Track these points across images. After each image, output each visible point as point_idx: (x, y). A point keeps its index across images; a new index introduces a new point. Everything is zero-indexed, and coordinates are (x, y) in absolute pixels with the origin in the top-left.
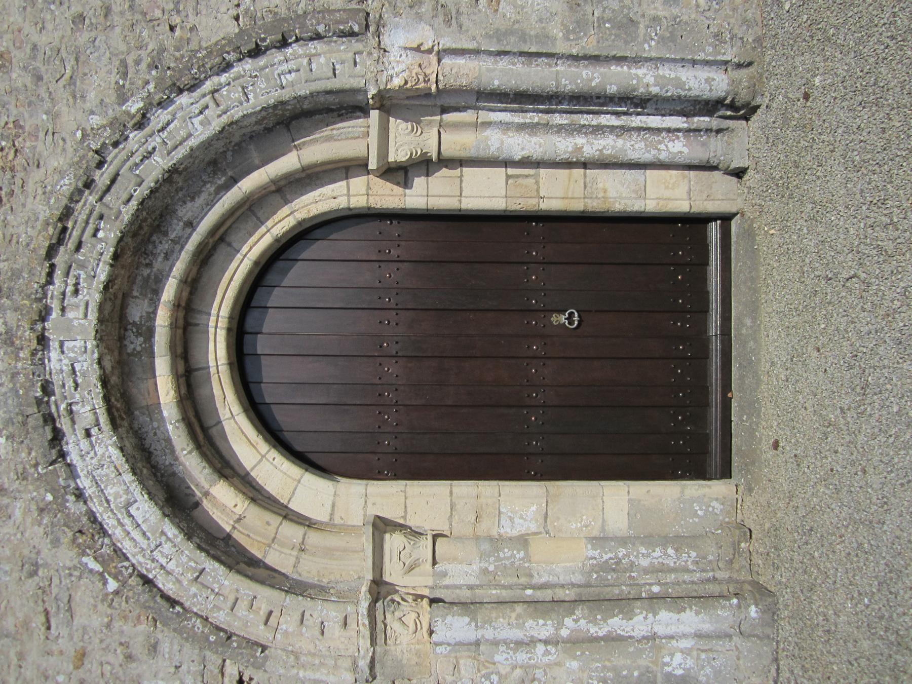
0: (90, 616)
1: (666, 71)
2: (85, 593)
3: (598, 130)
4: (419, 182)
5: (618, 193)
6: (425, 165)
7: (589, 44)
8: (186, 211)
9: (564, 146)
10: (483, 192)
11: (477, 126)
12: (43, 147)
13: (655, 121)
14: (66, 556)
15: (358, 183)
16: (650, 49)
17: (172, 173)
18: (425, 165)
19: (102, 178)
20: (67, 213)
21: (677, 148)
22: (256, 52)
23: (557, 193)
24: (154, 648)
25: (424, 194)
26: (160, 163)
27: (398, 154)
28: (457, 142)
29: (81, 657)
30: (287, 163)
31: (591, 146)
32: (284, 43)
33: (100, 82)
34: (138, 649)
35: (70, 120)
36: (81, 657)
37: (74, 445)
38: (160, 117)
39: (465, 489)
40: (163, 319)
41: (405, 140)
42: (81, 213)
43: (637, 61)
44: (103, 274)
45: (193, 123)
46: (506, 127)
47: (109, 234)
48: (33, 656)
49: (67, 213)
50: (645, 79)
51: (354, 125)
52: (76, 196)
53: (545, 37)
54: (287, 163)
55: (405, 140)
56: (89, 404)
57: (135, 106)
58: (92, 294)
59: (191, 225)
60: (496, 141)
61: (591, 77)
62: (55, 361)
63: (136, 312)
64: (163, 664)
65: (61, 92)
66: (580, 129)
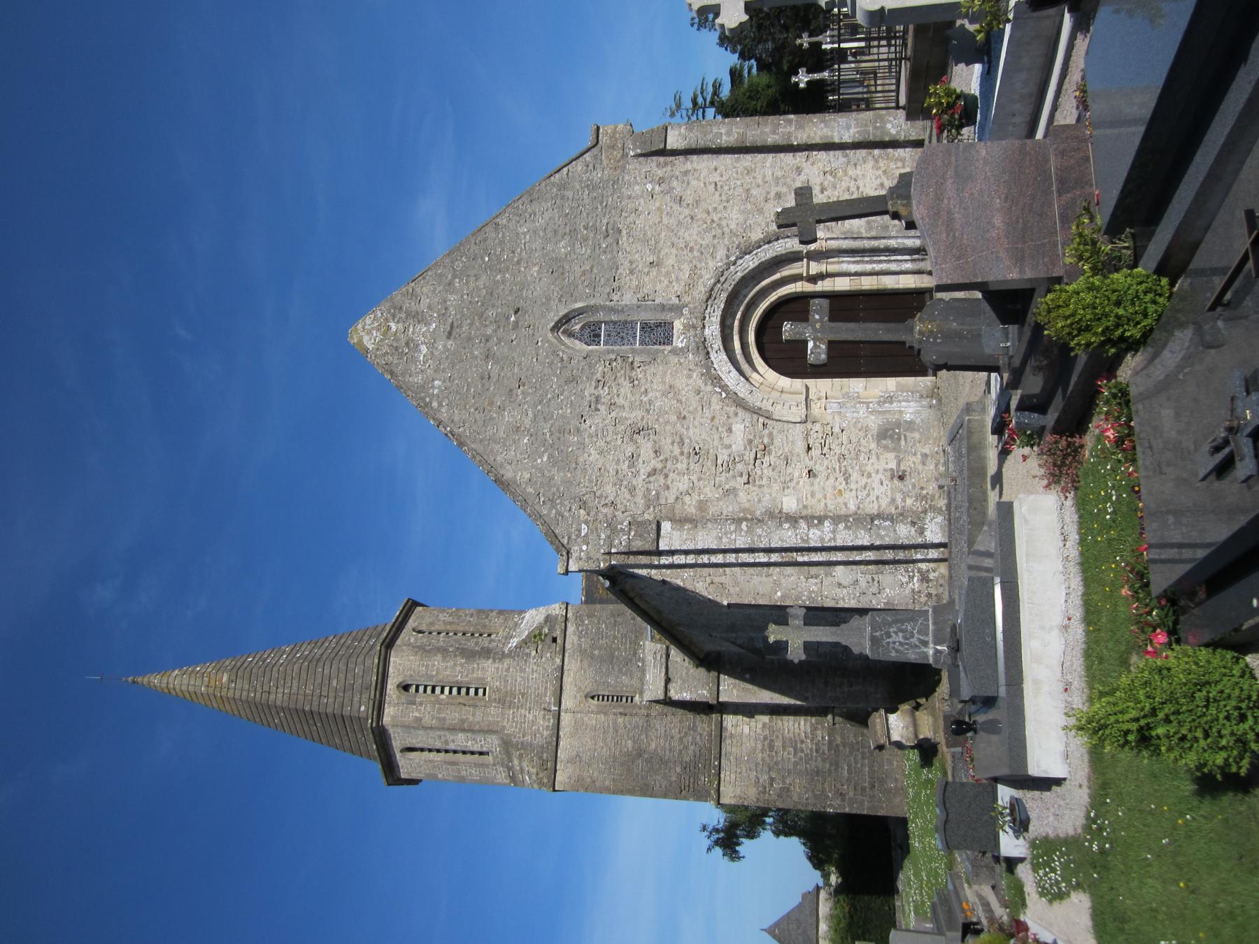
0: (716, 406)
1: (900, 241)
2: (715, 399)
3: (880, 262)
4: (820, 283)
5: (889, 283)
6: (821, 276)
7: (874, 234)
8: (744, 292)
9: (868, 267)
10: (842, 284)
11: (839, 263)
12: (703, 272)
13: (899, 258)
14: (709, 388)
15: (799, 284)
16: (893, 234)
17: (743, 278)
18: (821, 276)
19: (722, 279)
20: (712, 289)
21: (909, 266)
22: (769, 242)
23: (868, 283)
24: (736, 414)
25: (822, 286)
26: (740, 275)
27: (813, 272)
28: (832, 268)
29: (713, 418)
30: (777, 276)
31: (878, 267)
32: (777, 239)
33: (721, 253)
34: (731, 414)
35: (711, 264)
36: (713, 418)
37: (713, 356)
38: (740, 262)
39: (837, 381)
40: (736, 323)
41: (815, 268)
42: (716, 290)
43: (890, 238)
44: (722, 306)
45: (750, 262)
46: (849, 262)
47: (724, 296)
48: (698, 418)
49: (712, 289)
50: (893, 243)
51: (798, 264)
52: (715, 284)
53: (859, 232)
54: (777, 276)
55: (815, 268)
56: (718, 344)
57: (733, 259)
58: (719, 313)
59: (745, 297)
60: (845, 267)
61: (875, 243)
62: (707, 332)
63: (728, 322)
64: (739, 419)
65: (708, 256)
66: (874, 262)
